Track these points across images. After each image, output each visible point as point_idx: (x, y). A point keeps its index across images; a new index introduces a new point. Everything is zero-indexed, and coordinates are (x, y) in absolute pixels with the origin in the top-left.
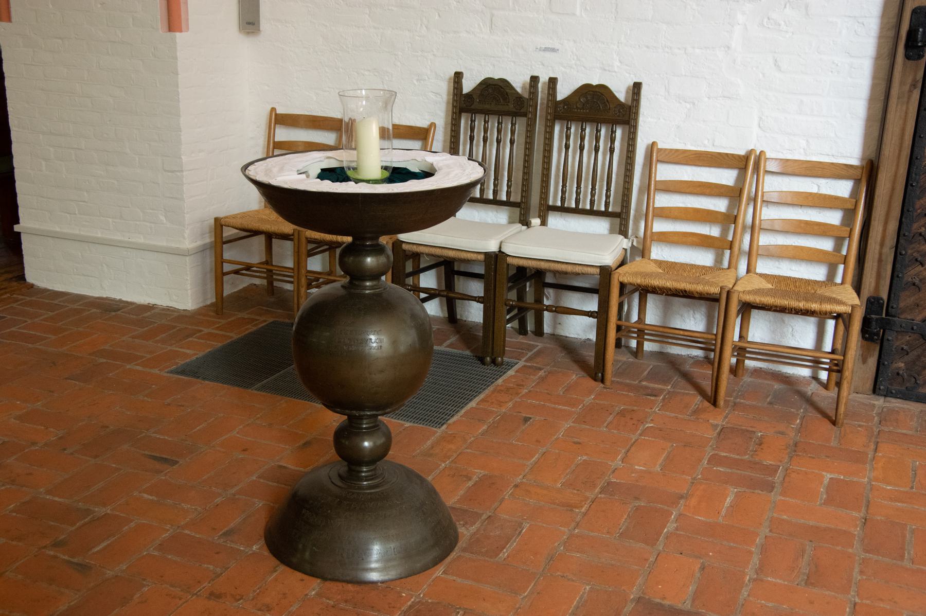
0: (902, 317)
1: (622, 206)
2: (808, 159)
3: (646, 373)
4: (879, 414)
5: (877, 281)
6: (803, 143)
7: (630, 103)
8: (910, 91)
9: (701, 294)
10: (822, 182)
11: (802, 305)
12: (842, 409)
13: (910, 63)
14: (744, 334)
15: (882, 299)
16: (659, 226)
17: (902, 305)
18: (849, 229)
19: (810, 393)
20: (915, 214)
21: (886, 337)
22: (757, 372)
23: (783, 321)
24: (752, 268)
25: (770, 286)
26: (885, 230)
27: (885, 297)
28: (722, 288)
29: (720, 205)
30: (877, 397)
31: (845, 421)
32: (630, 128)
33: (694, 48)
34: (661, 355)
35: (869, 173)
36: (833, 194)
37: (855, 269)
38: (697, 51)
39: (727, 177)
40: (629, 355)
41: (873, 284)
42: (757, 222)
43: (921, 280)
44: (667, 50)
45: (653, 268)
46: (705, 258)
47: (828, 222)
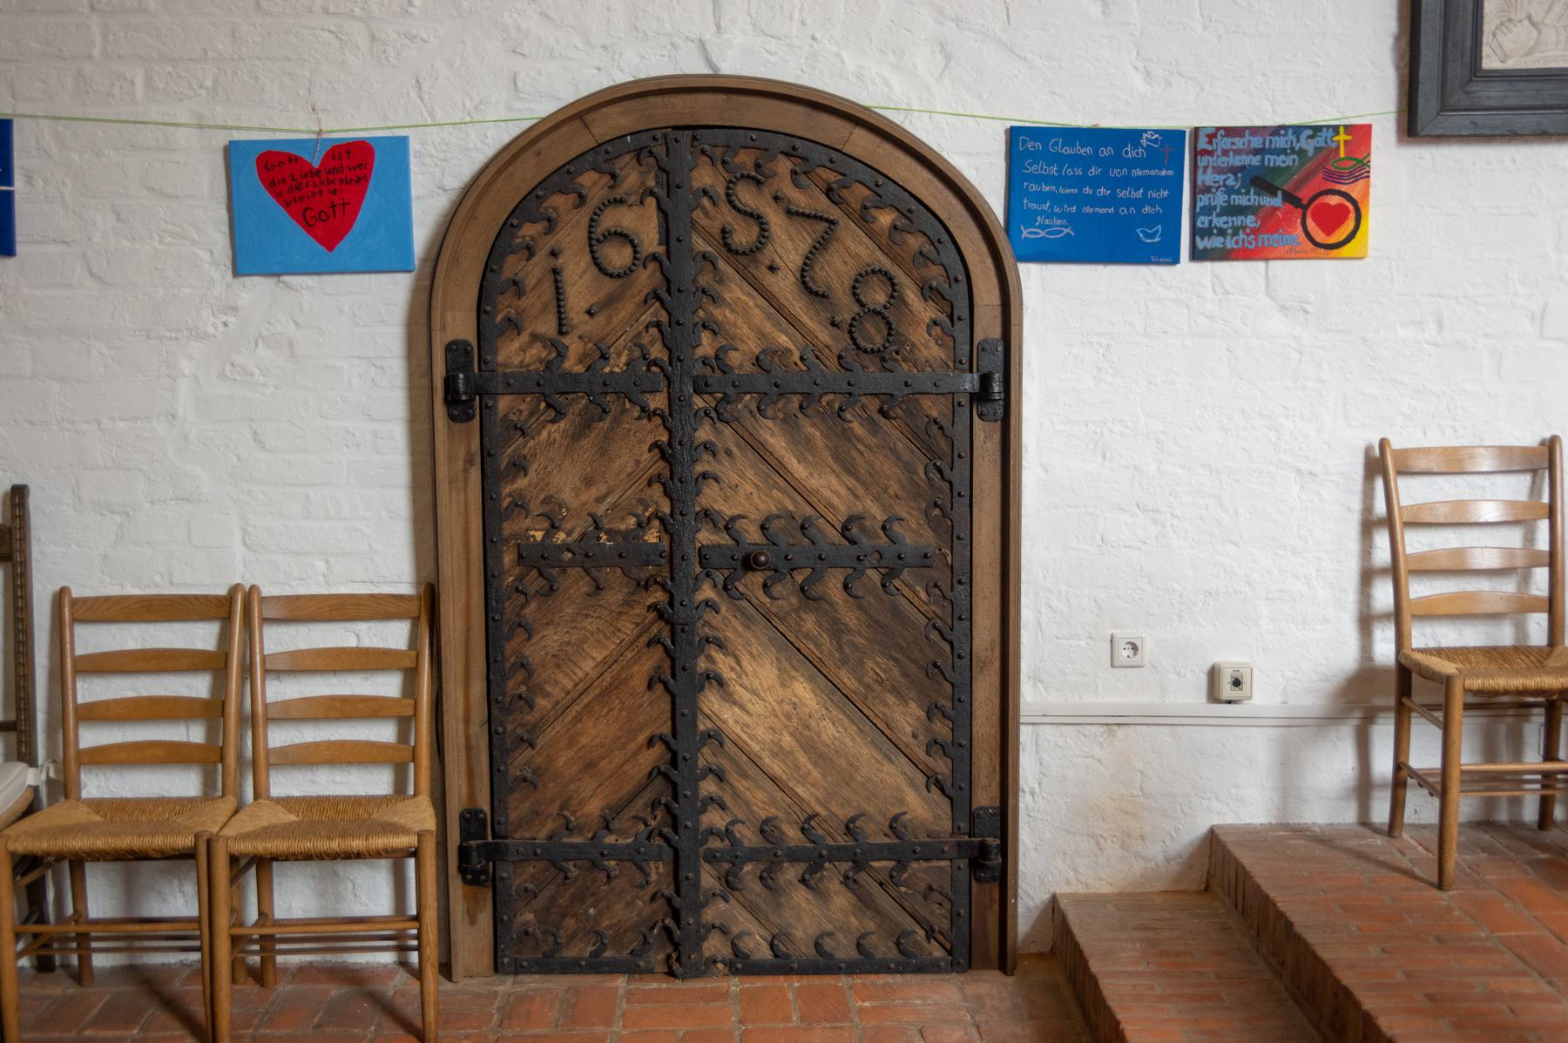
0: (517, 836)
1: (18, 709)
2: (333, 591)
3: (94, 1012)
4: (501, 1009)
5: (468, 787)
6: (321, 566)
7: (9, 524)
8: (466, 471)
9: (162, 851)
10: (362, 627)
11: (335, 845)
12: (431, 1013)
13: (458, 426)
14: (266, 910)
15: (482, 811)
16: (91, 737)
17: (513, 816)
18: (411, 702)
19: (391, 994)
20: (507, 666)
21: (498, 873)
22: (304, 972)
23: (336, 874)
24: (262, 790)
25: (292, 818)
26: (467, 696)
27: (486, 807)
28: (197, 836)
29: (198, 686)
30: (503, 978)
31: (441, 1033)
32: (14, 568)
33: (113, 419)
34: (133, 973)
35: (427, 606)
36: (381, 645)
37: (432, 768)
38: (120, 424)
39: (201, 636)
40: (69, 982)
41: (465, 789)
42: (260, 709)
43: (534, 772)
44: (66, 425)
45: (82, 815)
46: (184, 783)
47: (382, 694)
